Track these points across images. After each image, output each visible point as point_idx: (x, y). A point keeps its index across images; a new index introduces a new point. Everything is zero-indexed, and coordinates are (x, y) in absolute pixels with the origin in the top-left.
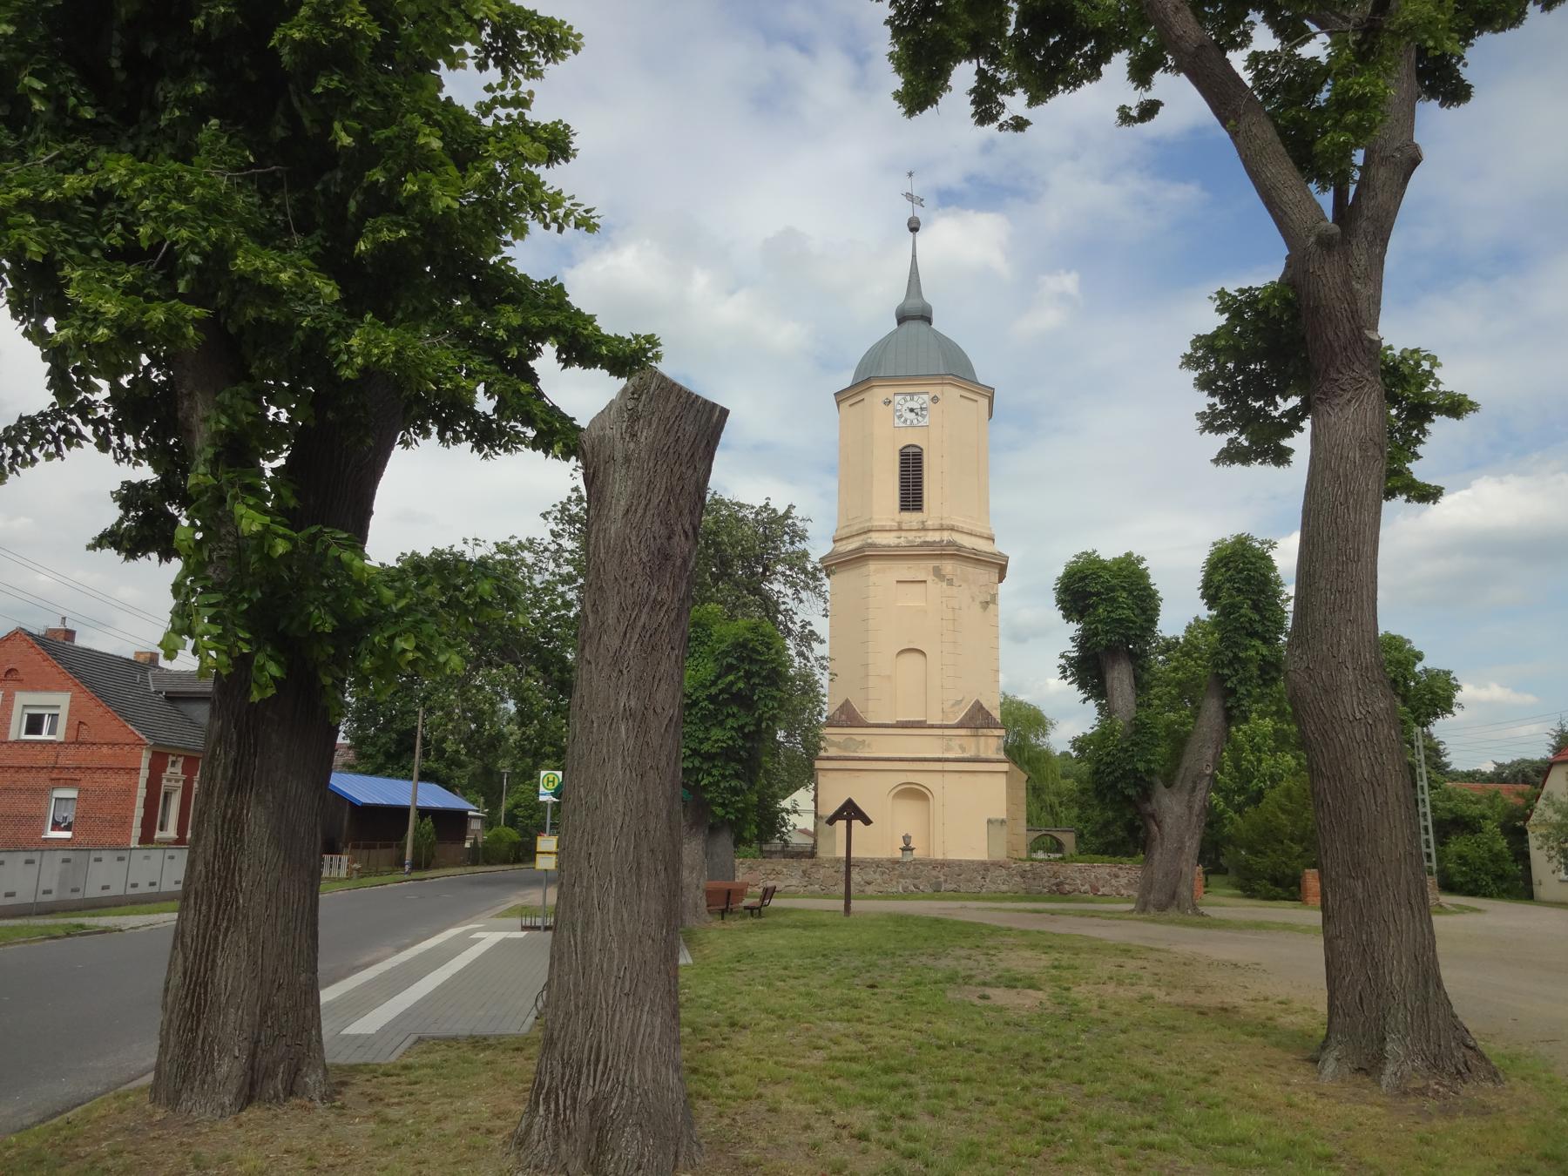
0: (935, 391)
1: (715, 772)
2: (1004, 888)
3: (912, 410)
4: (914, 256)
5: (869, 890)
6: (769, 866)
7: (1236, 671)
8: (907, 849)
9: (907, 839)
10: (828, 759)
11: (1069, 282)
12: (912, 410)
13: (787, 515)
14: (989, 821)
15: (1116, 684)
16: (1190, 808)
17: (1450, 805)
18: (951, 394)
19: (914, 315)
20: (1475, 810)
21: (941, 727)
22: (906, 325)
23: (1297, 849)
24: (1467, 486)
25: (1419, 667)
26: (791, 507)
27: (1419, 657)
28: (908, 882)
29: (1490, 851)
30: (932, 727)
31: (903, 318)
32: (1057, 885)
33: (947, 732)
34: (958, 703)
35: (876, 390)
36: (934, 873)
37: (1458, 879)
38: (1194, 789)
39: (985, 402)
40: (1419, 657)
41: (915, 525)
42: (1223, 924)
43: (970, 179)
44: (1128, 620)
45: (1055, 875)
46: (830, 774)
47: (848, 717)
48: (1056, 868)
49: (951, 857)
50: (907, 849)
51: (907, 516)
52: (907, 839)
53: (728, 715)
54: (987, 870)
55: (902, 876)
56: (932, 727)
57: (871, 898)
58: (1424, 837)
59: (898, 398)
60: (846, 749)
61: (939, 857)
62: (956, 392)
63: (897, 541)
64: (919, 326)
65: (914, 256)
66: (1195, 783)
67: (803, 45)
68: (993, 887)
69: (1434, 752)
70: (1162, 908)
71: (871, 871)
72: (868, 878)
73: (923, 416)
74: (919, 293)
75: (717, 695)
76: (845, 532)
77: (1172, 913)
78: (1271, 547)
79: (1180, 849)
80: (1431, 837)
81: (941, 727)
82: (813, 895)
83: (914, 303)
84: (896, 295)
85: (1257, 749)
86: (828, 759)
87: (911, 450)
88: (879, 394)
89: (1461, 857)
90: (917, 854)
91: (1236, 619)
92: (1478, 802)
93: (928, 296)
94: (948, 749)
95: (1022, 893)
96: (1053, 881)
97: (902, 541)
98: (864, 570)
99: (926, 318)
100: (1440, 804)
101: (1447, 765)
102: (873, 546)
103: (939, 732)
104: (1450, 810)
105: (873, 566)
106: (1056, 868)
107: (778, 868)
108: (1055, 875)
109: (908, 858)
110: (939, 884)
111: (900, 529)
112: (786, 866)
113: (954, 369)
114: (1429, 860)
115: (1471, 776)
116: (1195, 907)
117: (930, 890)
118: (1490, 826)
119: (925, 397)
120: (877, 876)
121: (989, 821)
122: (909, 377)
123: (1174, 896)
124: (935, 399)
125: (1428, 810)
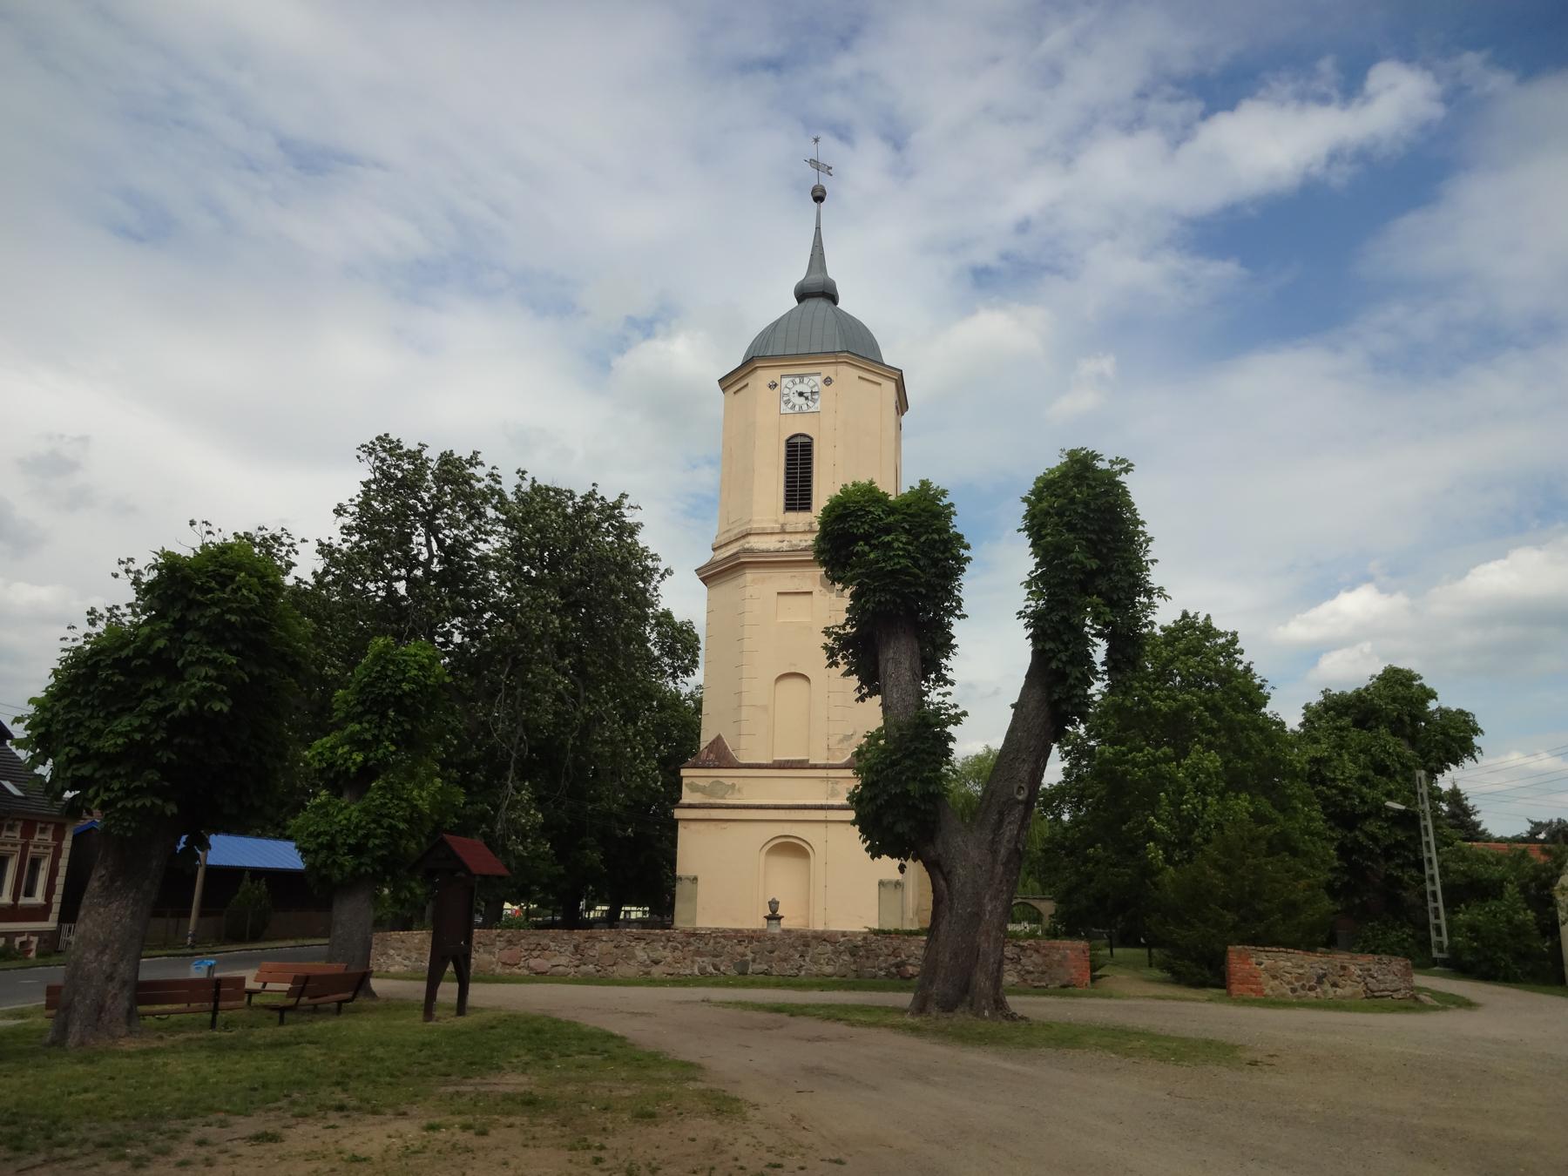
0: (828, 371)
1: (116, 785)
2: (828, 969)
3: (801, 394)
4: (818, 228)
5: (656, 971)
6: (533, 939)
7: (1066, 644)
8: (774, 917)
9: (774, 905)
10: (691, 806)
11: (1107, 364)
12: (801, 394)
13: (617, 505)
14: (881, 883)
15: (890, 667)
16: (994, 852)
17: (1463, 867)
18: (847, 375)
19: (817, 292)
20: (1496, 872)
21: (825, 767)
22: (811, 304)
23: (1230, 917)
24: (1505, 557)
25: (1432, 705)
26: (624, 496)
27: (1432, 695)
28: (706, 962)
29: (1509, 921)
30: (815, 767)
31: (802, 294)
32: (897, 966)
33: (832, 773)
34: (847, 738)
35: (760, 372)
36: (740, 949)
37: (1467, 958)
38: (1000, 822)
39: (890, 387)
40: (1432, 695)
41: (801, 528)
42: (1067, 1038)
43: (1005, 257)
44: (904, 571)
45: (895, 953)
46: (693, 826)
47: (722, 757)
48: (896, 943)
49: (834, 927)
50: (774, 917)
51: (792, 516)
52: (774, 905)
53: (148, 693)
54: (807, 945)
55: (698, 953)
56: (815, 767)
57: (661, 983)
58: (1431, 905)
59: (786, 381)
60: (711, 795)
61: (820, 927)
62: (853, 373)
63: (778, 545)
64: (822, 304)
65: (818, 228)
66: (1001, 814)
67: (843, 133)
68: (815, 969)
69: (1459, 813)
70: (948, 1007)
71: (659, 945)
72: (655, 955)
73: (814, 401)
74: (823, 269)
75: (128, 659)
76: (723, 539)
77: (960, 1017)
78: (1127, 470)
79: (977, 916)
80: (1440, 904)
81: (825, 767)
82: (587, 980)
83: (816, 277)
84: (798, 272)
85: (1202, 789)
86: (691, 806)
87: (799, 440)
88: (763, 377)
89: (1472, 928)
90: (785, 924)
91: (1063, 566)
92: (1499, 863)
93: (832, 273)
94: (834, 794)
95: (852, 976)
96: (892, 960)
97: (785, 546)
98: (740, 581)
99: (830, 296)
100: (1452, 866)
101: (1478, 824)
102: (750, 551)
103: (822, 773)
104: (1464, 873)
105: (750, 575)
106: (896, 943)
107: (544, 942)
108: (895, 953)
109: (775, 930)
110: (745, 964)
111: (783, 532)
112: (553, 939)
113: (858, 348)
114: (1439, 933)
115: (1499, 840)
116: (999, 1005)
117: (733, 972)
118: (1511, 890)
119: (818, 379)
120: (667, 953)
121: (881, 883)
122: (797, 356)
123: (965, 988)
124: (828, 381)
125: (1436, 871)
